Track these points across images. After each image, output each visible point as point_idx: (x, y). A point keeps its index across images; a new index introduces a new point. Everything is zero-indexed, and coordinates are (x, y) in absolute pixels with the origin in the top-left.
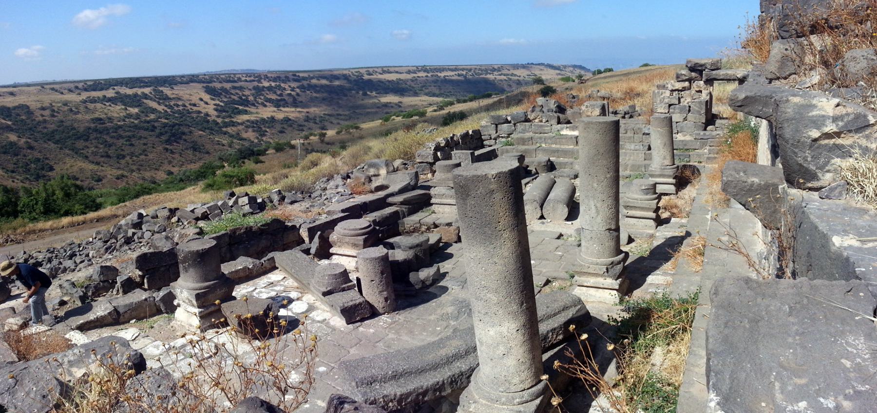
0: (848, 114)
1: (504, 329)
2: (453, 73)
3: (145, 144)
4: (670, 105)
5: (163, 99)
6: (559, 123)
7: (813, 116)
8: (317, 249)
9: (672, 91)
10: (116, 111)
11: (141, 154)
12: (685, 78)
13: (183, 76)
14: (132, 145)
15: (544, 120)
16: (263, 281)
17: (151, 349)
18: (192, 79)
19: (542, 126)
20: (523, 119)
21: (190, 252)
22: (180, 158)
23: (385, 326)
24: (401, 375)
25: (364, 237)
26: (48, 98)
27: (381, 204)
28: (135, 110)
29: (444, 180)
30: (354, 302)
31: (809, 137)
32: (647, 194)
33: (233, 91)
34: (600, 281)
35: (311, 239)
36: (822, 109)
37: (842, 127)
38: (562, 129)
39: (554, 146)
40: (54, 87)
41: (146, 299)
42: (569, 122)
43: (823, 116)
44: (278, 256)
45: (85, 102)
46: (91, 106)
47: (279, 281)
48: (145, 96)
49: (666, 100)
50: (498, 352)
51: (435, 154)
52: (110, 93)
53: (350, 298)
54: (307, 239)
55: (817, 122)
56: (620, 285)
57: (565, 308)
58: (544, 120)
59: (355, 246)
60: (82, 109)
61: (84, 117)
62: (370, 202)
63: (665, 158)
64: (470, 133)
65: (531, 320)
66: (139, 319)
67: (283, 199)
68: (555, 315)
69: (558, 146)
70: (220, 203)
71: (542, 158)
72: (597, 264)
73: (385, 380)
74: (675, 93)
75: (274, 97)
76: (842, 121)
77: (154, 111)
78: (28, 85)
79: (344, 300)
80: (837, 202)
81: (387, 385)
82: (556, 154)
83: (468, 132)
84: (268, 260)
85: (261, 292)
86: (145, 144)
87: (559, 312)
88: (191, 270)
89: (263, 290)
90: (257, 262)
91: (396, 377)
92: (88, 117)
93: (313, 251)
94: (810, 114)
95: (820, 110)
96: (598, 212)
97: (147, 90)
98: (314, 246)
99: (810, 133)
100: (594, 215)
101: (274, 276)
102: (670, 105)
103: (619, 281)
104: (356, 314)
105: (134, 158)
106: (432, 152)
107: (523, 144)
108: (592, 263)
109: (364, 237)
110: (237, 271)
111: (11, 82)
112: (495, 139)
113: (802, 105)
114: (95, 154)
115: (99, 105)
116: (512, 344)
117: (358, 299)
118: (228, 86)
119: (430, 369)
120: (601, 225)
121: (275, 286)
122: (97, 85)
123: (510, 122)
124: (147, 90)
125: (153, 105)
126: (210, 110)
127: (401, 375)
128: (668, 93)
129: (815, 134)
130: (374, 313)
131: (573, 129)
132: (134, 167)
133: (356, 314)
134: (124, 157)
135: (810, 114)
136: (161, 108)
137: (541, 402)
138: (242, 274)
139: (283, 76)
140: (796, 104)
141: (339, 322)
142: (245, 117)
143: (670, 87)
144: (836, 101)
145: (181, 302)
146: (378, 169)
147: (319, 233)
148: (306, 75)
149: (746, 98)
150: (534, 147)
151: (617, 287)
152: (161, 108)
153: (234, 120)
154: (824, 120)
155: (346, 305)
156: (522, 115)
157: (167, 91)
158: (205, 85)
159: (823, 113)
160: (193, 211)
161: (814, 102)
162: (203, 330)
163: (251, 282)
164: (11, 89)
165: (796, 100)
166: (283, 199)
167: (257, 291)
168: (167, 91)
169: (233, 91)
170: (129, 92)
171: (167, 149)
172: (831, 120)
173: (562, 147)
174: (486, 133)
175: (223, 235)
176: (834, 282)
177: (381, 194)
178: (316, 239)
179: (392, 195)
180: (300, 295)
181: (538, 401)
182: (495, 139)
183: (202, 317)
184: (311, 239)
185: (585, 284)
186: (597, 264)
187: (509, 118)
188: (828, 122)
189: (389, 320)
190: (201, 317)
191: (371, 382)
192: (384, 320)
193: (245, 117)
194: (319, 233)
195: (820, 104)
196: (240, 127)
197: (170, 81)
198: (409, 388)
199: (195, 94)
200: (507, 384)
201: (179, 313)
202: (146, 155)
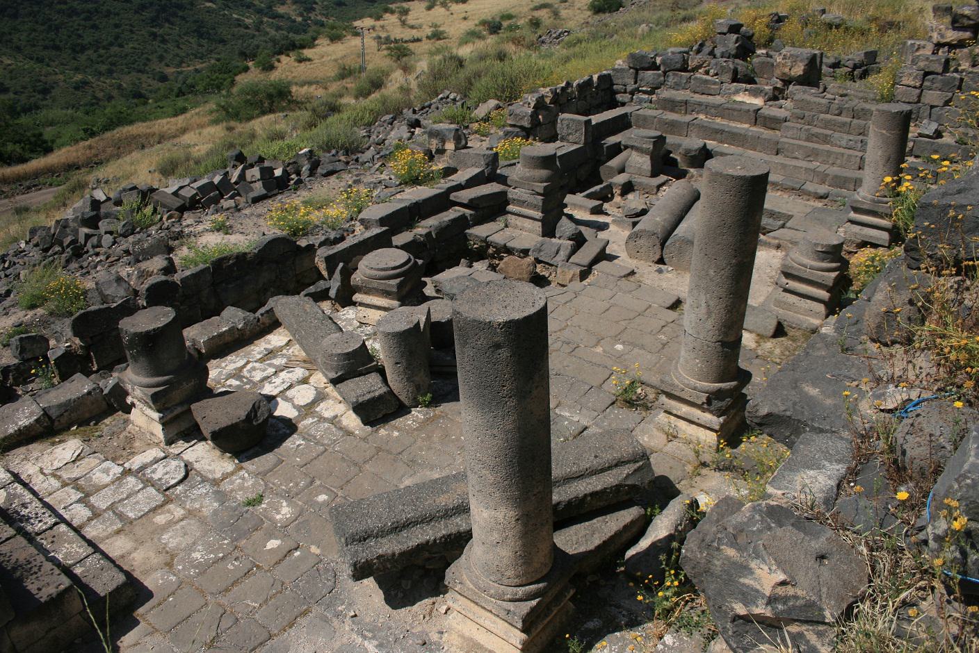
0: (796, 597)
3: (117, 26)
4: (927, 74)
6: (735, 79)
7: (744, 585)
8: (338, 290)
9: (939, 45)
11: (111, 44)
12: (966, 22)
14: (94, 27)
15: (712, 72)
16: (258, 348)
17: (98, 474)
19: (706, 81)
20: (678, 66)
21: (136, 334)
22: (177, 51)
23: (415, 425)
24: (404, 527)
25: (398, 281)
27: (441, 203)
29: (528, 179)
30: (372, 395)
31: (732, 609)
32: (823, 260)
34: (696, 413)
35: (331, 272)
36: (757, 580)
37: (782, 612)
38: (737, 92)
39: (718, 120)
41: (89, 393)
42: (751, 81)
43: (757, 591)
44: (281, 305)
47: (281, 348)
49: (922, 64)
51: (534, 115)
53: (369, 386)
54: (325, 273)
55: (748, 596)
56: (722, 426)
57: (619, 463)
58: (712, 72)
59: (386, 293)
62: (425, 201)
64: (595, 78)
66: (83, 423)
67: (315, 166)
68: (603, 470)
69: (725, 122)
70: (217, 179)
71: (694, 142)
72: (695, 389)
73: (382, 533)
74: (942, 52)
76: (785, 603)
79: (359, 392)
81: (384, 540)
82: (719, 136)
83: (591, 79)
84: (267, 312)
85: (254, 369)
86: (117, 26)
87: (610, 468)
88: (142, 359)
89: (257, 365)
90: (251, 316)
91: (397, 528)
93: (332, 293)
94: (742, 580)
95: (755, 579)
96: (709, 313)
98: (334, 285)
99: (734, 605)
101: (276, 339)
102: (927, 74)
103: (721, 419)
104: (376, 412)
105: (102, 51)
106: (530, 111)
107: (672, 110)
108: (687, 386)
109: (398, 281)
110: (221, 335)
112: (632, 93)
113: (735, 563)
117: (380, 389)
120: (711, 333)
121: (275, 357)
123: (658, 68)
127: (404, 527)
128: (929, 49)
129: (740, 609)
130: (401, 410)
131: (755, 93)
132: (103, 68)
133: (376, 412)
134: (83, 49)
135: (742, 580)
137: (538, 603)
138: (228, 339)
140: (728, 558)
141: (352, 421)
143: (936, 37)
144: (781, 577)
145: (135, 401)
146: (443, 142)
147: (341, 265)
149: (769, 415)
150: (688, 118)
151: (717, 427)
154: (756, 598)
155: (361, 400)
156: (678, 58)
159: (758, 587)
160: (175, 194)
161: (753, 565)
162: (170, 442)
163: (242, 352)
165: (731, 552)
166: (315, 166)
167: (249, 367)
171: (154, 35)
172: (765, 601)
173: (733, 124)
174: (620, 81)
175: (202, 271)
177: (443, 185)
178: (337, 275)
179: (459, 187)
180: (307, 373)
181: (534, 603)
182: (632, 93)
183: (165, 424)
184: (331, 272)
185: (675, 412)
186: (695, 389)
187: (658, 60)
188: (761, 602)
189: (421, 416)
190: (163, 424)
191: (363, 538)
192: (417, 414)
194: (341, 265)
195: (758, 572)
198: (410, 544)
201: (135, 415)
202: (121, 46)
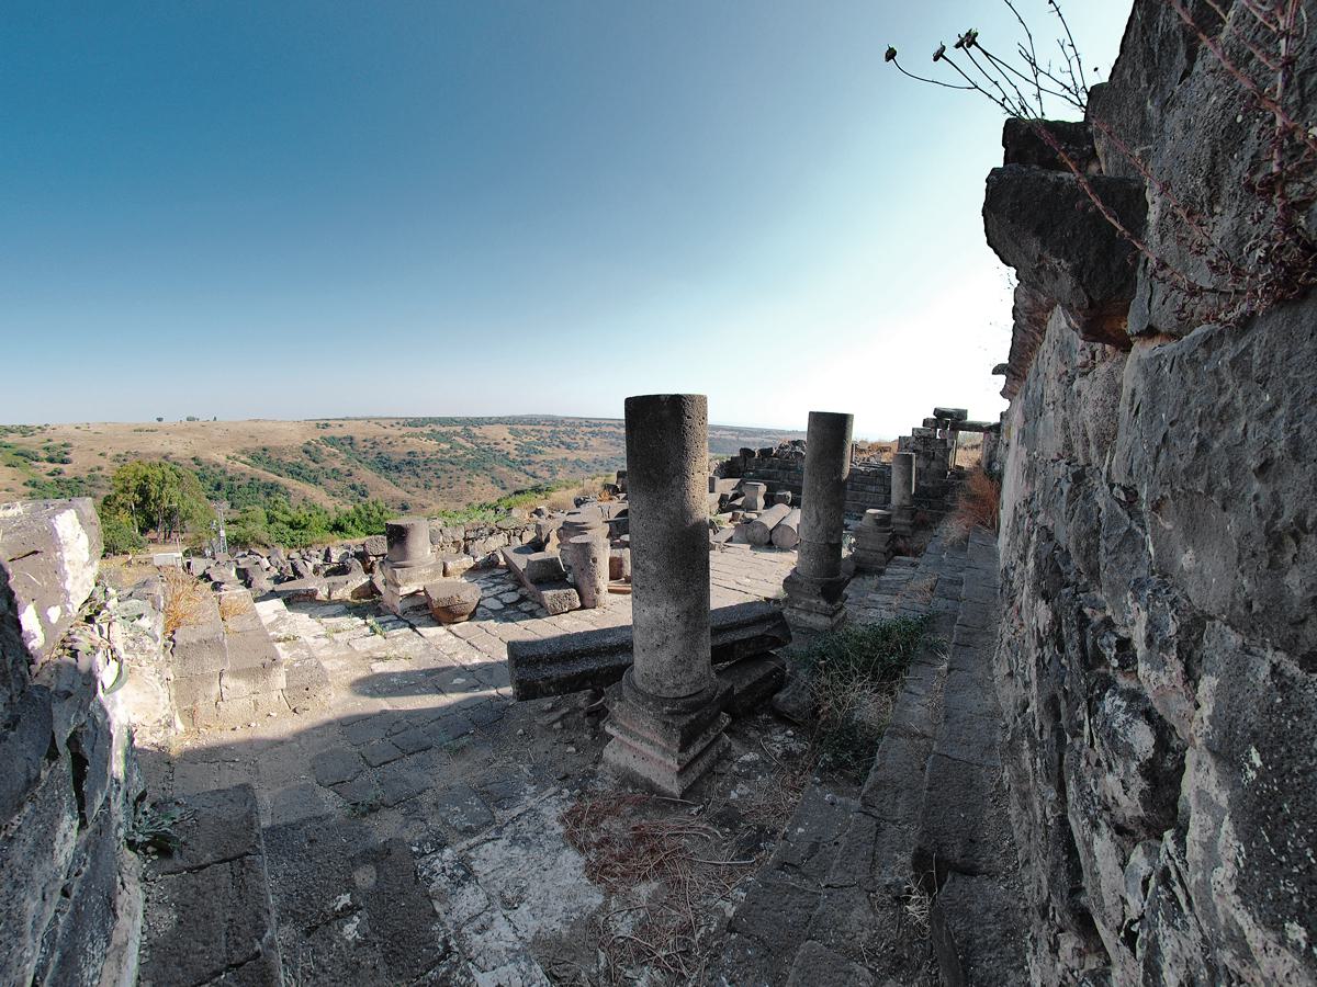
1: (661, 611)
2: (728, 433)
5: (470, 436)
10: (431, 446)
13: (491, 418)
18: (499, 421)
28: (446, 446)
45: (402, 436)
46: (409, 440)
48: (456, 434)
50: (652, 641)
52: (426, 430)
63: (904, 498)
75: (568, 440)
78: (356, 419)
80: (1227, 27)
96: (819, 520)
97: (459, 429)
100: (814, 524)
111: (344, 417)
114: (959, 764)
116: (670, 633)
118: (528, 428)
124: (459, 429)
125: (462, 441)
126: (511, 448)
136: (469, 445)
139: (577, 423)
142: (543, 457)
152: (469, 445)
153: (532, 459)
157: (475, 431)
164: (340, 422)
168: (475, 431)
169: (533, 433)
170: (444, 430)
193: (543, 457)
196: (537, 466)
197: (479, 422)
199: (502, 432)
200: (658, 686)
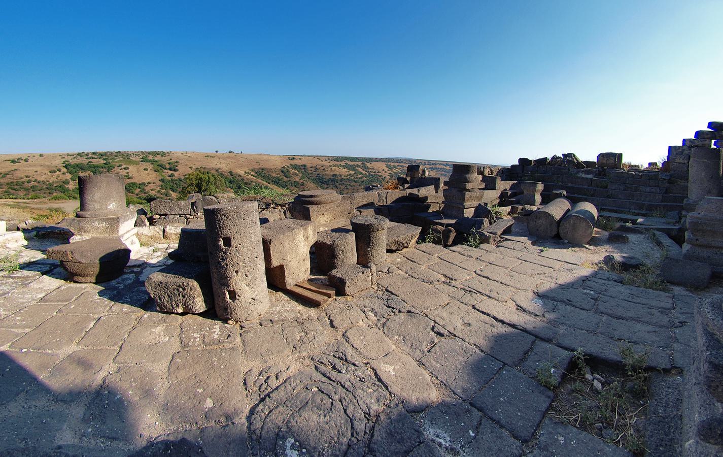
5: (365, 168)
10: (344, 171)
13: (376, 158)
18: (381, 160)
26: (316, 162)
33: (398, 167)
40: (318, 157)
48: (358, 166)
52: (343, 163)
60: (329, 169)
61: (329, 173)
65: (236, 184)
77: (361, 173)
78: (308, 156)
92: (332, 173)
97: (360, 163)
109: (501, 329)
111: (319, 155)
115: (337, 168)
119: (291, 294)
122: (338, 159)
124: (360, 163)
125: (361, 170)
136: (364, 172)
148: (434, 162)
152: (364, 172)
157: (368, 165)
158: (386, 163)
168: (368, 165)
176: (708, 444)
197: (370, 160)
